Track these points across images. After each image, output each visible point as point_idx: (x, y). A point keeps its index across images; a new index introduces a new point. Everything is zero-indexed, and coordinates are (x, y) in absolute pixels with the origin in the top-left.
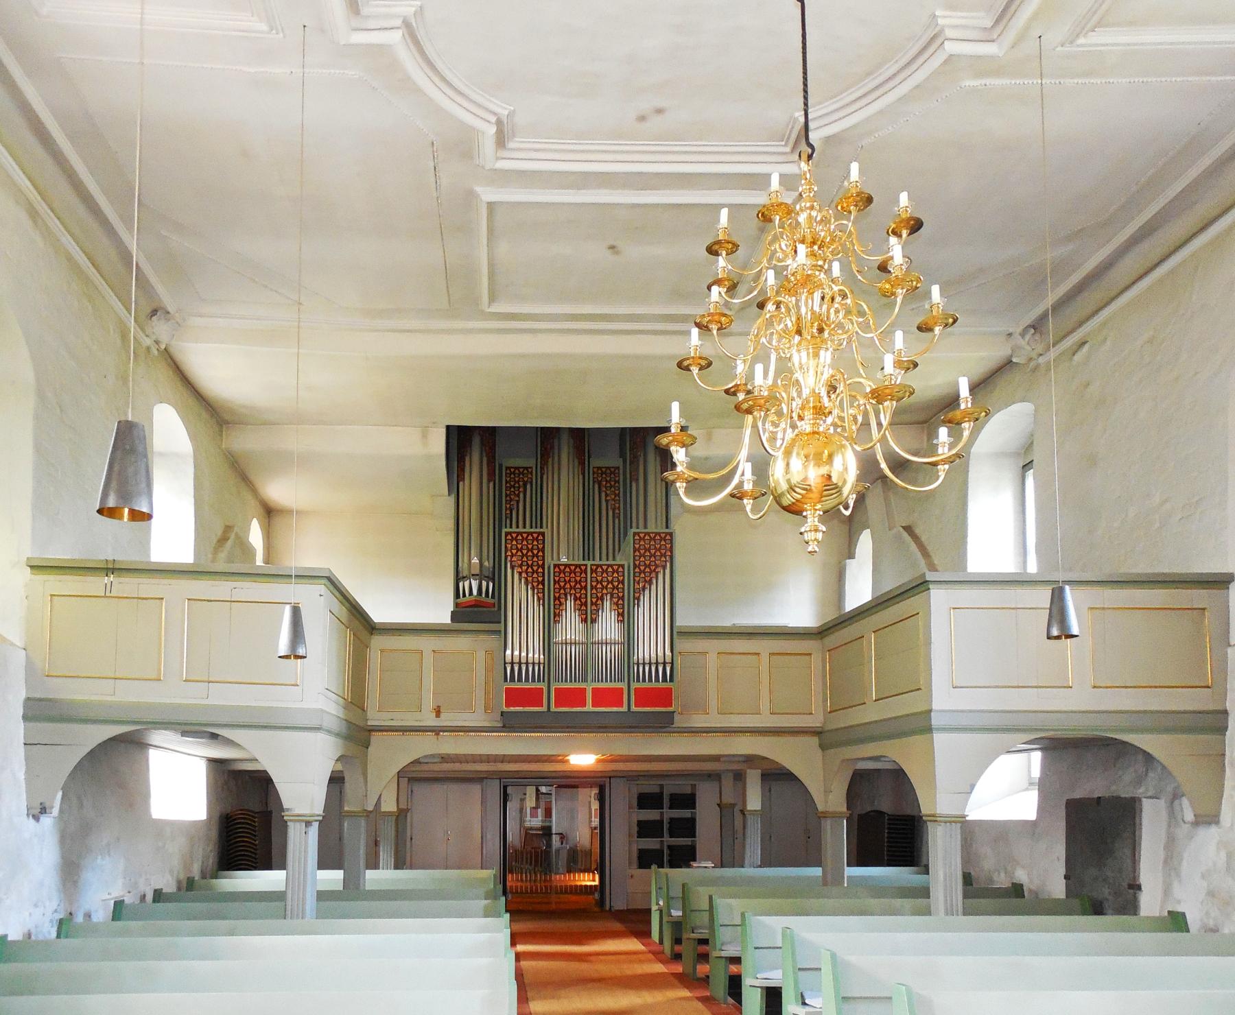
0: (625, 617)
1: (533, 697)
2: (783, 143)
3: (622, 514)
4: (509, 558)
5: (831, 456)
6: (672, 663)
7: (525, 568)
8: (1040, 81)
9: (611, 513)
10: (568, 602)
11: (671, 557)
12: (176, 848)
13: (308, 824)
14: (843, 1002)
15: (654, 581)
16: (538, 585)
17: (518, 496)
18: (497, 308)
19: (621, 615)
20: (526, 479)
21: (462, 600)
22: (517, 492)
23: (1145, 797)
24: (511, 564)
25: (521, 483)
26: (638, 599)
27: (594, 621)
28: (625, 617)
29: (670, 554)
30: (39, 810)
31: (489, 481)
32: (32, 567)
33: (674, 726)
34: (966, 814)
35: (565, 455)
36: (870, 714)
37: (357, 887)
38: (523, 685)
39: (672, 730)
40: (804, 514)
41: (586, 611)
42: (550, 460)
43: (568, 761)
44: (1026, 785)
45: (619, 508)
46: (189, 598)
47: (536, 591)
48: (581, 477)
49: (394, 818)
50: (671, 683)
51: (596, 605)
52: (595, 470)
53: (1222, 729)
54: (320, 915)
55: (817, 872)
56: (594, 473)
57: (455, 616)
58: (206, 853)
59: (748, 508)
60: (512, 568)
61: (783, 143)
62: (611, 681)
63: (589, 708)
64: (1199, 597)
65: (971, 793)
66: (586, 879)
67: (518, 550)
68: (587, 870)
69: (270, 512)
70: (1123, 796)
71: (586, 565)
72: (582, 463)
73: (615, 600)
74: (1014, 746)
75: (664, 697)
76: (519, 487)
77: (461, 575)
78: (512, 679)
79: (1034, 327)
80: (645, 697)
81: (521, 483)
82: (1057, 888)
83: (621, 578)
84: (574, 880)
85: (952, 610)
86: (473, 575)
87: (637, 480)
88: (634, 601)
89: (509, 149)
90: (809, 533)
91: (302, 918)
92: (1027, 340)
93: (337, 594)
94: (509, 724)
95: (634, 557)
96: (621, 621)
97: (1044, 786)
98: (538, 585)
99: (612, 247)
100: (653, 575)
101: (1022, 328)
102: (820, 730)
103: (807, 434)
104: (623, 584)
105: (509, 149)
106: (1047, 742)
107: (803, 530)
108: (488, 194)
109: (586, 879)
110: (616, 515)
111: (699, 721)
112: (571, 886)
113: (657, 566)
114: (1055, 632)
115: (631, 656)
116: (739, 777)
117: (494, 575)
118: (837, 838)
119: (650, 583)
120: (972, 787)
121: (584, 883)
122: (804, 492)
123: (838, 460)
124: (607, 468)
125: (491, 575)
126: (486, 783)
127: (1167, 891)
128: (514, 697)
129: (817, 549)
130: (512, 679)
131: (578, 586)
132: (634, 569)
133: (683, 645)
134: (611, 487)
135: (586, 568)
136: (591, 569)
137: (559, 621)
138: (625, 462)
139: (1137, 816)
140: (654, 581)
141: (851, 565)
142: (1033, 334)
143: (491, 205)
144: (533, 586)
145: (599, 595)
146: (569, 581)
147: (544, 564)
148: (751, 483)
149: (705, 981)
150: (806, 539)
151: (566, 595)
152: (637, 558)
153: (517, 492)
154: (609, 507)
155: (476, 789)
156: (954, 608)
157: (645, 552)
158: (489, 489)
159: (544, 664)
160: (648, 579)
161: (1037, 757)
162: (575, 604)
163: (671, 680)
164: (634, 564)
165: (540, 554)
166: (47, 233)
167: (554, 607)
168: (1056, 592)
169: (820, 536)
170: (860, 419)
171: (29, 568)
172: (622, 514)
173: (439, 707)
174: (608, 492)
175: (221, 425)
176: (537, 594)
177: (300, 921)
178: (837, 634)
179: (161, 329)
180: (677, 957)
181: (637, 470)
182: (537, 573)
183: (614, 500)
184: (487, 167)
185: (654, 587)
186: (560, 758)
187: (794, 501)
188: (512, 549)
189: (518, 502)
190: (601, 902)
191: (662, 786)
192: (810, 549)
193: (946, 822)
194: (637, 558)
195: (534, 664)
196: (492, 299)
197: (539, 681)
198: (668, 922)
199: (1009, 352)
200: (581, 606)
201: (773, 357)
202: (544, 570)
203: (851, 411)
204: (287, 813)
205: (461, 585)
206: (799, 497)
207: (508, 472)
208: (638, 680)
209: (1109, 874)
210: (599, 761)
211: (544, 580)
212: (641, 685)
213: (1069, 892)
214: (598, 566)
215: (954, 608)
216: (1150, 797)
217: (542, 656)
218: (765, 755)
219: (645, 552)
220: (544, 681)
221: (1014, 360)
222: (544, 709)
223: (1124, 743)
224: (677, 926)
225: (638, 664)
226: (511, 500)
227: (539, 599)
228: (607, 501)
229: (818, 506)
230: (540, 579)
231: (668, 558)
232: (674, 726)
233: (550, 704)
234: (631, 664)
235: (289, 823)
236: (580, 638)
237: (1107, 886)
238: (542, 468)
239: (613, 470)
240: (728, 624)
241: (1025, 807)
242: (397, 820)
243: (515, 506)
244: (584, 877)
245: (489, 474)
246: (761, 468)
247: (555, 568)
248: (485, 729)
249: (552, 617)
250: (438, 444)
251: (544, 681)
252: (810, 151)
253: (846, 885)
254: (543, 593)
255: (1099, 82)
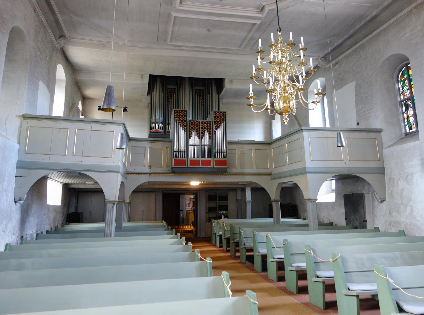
0: (212, 138)
1: (183, 163)
2: (258, 9)
3: (204, 104)
4: (175, 118)
5: (289, 102)
6: (226, 152)
7: (180, 121)
8: (323, 1)
9: (201, 104)
10: (194, 132)
11: (225, 119)
12: (52, 215)
13: (114, 204)
14: (291, 255)
15: (220, 126)
16: (184, 127)
17: (171, 97)
18: (173, 43)
19: (210, 137)
20: (174, 92)
21: (152, 130)
22: (171, 96)
23: (366, 193)
24: (176, 120)
25: (172, 93)
26: (216, 132)
27: (202, 139)
28: (212, 138)
29: (225, 118)
30: (19, 200)
31: (162, 92)
32: (23, 117)
33: (227, 172)
34: (317, 198)
35: (187, 86)
36: (285, 169)
37: (121, 228)
38: (179, 159)
39: (226, 173)
40: (284, 115)
41: (200, 135)
42: (182, 87)
43: (190, 184)
44: (331, 192)
45: (203, 102)
46: (31, 126)
47: (184, 129)
48: (192, 92)
49: (128, 205)
50: (226, 159)
51: (203, 134)
52: (196, 90)
53: (383, 173)
54: (116, 236)
55: (271, 220)
56: (196, 91)
57: (150, 136)
58: (60, 218)
59: (269, 112)
60: (176, 121)
61: (258, 9)
62: (207, 158)
63: (201, 166)
64: (373, 135)
65: (318, 192)
66: (188, 228)
67: (178, 116)
68: (188, 224)
69: (84, 99)
70: (359, 193)
71: (199, 121)
72: (192, 88)
73: (208, 132)
74: (329, 178)
75: (224, 163)
76: (172, 95)
77: (152, 122)
78: (176, 157)
79: (323, 57)
80: (218, 163)
81: (172, 93)
82: (343, 222)
83: (210, 125)
84: (184, 228)
85: (309, 138)
86: (156, 122)
87: (209, 94)
88: (214, 133)
89: (183, 4)
90: (285, 120)
91: (110, 237)
92: (322, 61)
93: (124, 128)
94: (174, 172)
95: (214, 119)
96: (210, 139)
97: (337, 191)
98: (184, 127)
99: (208, 30)
100: (220, 125)
101: (320, 57)
102: (271, 173)
103: (283, 96)
104: (211, 127)
105: (183, 4)
106: (338, 177)
107: (283, 119)
108: (174, 14)
109: (188, 228)
110: (202, 104)
111: (234, 170)
112: (185, 230)
113: (221, 122)
114: (339, 145)
115: (214, 150)
116: (243, 190)
117: (166, 122)
118: (277, 209)
119: (219, 127)
120: (319, 190)
121: (188, 229)
122: (283, 110)
123: (291, 103)
124: (200, 90)
125: (162, 122)
126: (115, 198)
127: (374, 223)
128: (177, 163)
129: (287, 124)
130: (176, 157)
131: (197, 127)
132: (214, 123)
133: (229, 146)
134: (201, 96)
135: (199, 122)
136: (201, 122)
137: (191, 138)
138: (205, 88)
139: (364, 199)
140: (220, 126)
141: (274, 122)
142: (323, 60)
143: (175, 17)
144: (183, 127)
145: (204, 130)
146: (194, 126)
147: (186, 120)
148: (270, 106)
149: (238, 257)
150: (284, 122)
151: (193, 130)
152: (215, 119)
153: (171, 96)
154: (200, 102)
155: (153, 195)
156: (310, 137)
157: (217, 118)
158: (162, 94)
159: (186, 152)
160: (218, 126)
161: (334, 182)
162: (196, 133)
163: (226, 157)
164: (214, 121)
165: (185, 117)
166: (38, 16)
167: (200, 136)
168: (339, 134)
169: (288, 121)
170: (296, 93)
171: (23, 118)
172: (204, 104)
173: (151, 166)
174: (200, 97)
175: (74, 71)
176: (184, 130)
177: (110, 238)
178: (30, 113)
179: (62, 41)
180: (228, 251)
181: (209, 91)
182: (184, 123)
183: (202, 100)
184: (176, 8)
185: (220, 128)
186: (182, 183)
187: (281, 112)
188: (176, 115)
189: (171, 99)
190: (196, 235)
191: (216, 193)
192: (285, 124)
193: (312, 201)
194: (215, 119)
195: (185, 152)
196: (171, 41)
197: (185, 157)
198: (224, 239)
199: (317, 63)
200: (198, 134)
201: (274, 76)
202: (186, 122)
203: (294, 91)
204: (106, 200)
205: (152, 125)
206: (282, 111)
207: (168, 89)
208: (216, 158)
209: (358, 217)
210: (200, 184)
211: (186, 125)
212: (217, 159)
213: (347, 224)
214: (203, 121)
215: (310, 137)
216: (367, 193)
217: (185, 150)
218: (255, 182)
219: (217, 118)
220: (186, 157)
221: (319, 66)
222: (187, 167)
223: (359, 177)
224: (228, 240)
225: (216, 152)
226: (169, 98)
227: (185, 131)
228: (200, 100)
229: (287, 114)
230: (185, 125)
231: (224, 120)
232: (227, 172)
233: (188, 165)
234: (214, 152)
235: (107, 204)
236: (198, 143)
237: (357, 221)
238: (179, 89)
239: (201, 90)
240: (237, 140)
241: (332, 198)
242: (129, 205)
243: (170, 100)
244: (187, 227)
245: (162, 90)
246: (272, 104)
247: (190, 122)
248: (169, 173)
249: (189, 137)
250: (146, 81)
251: (186, 157)
252: (280, 30)
253: (281, 224)
254: (186, 129)
255: (337, 3)
